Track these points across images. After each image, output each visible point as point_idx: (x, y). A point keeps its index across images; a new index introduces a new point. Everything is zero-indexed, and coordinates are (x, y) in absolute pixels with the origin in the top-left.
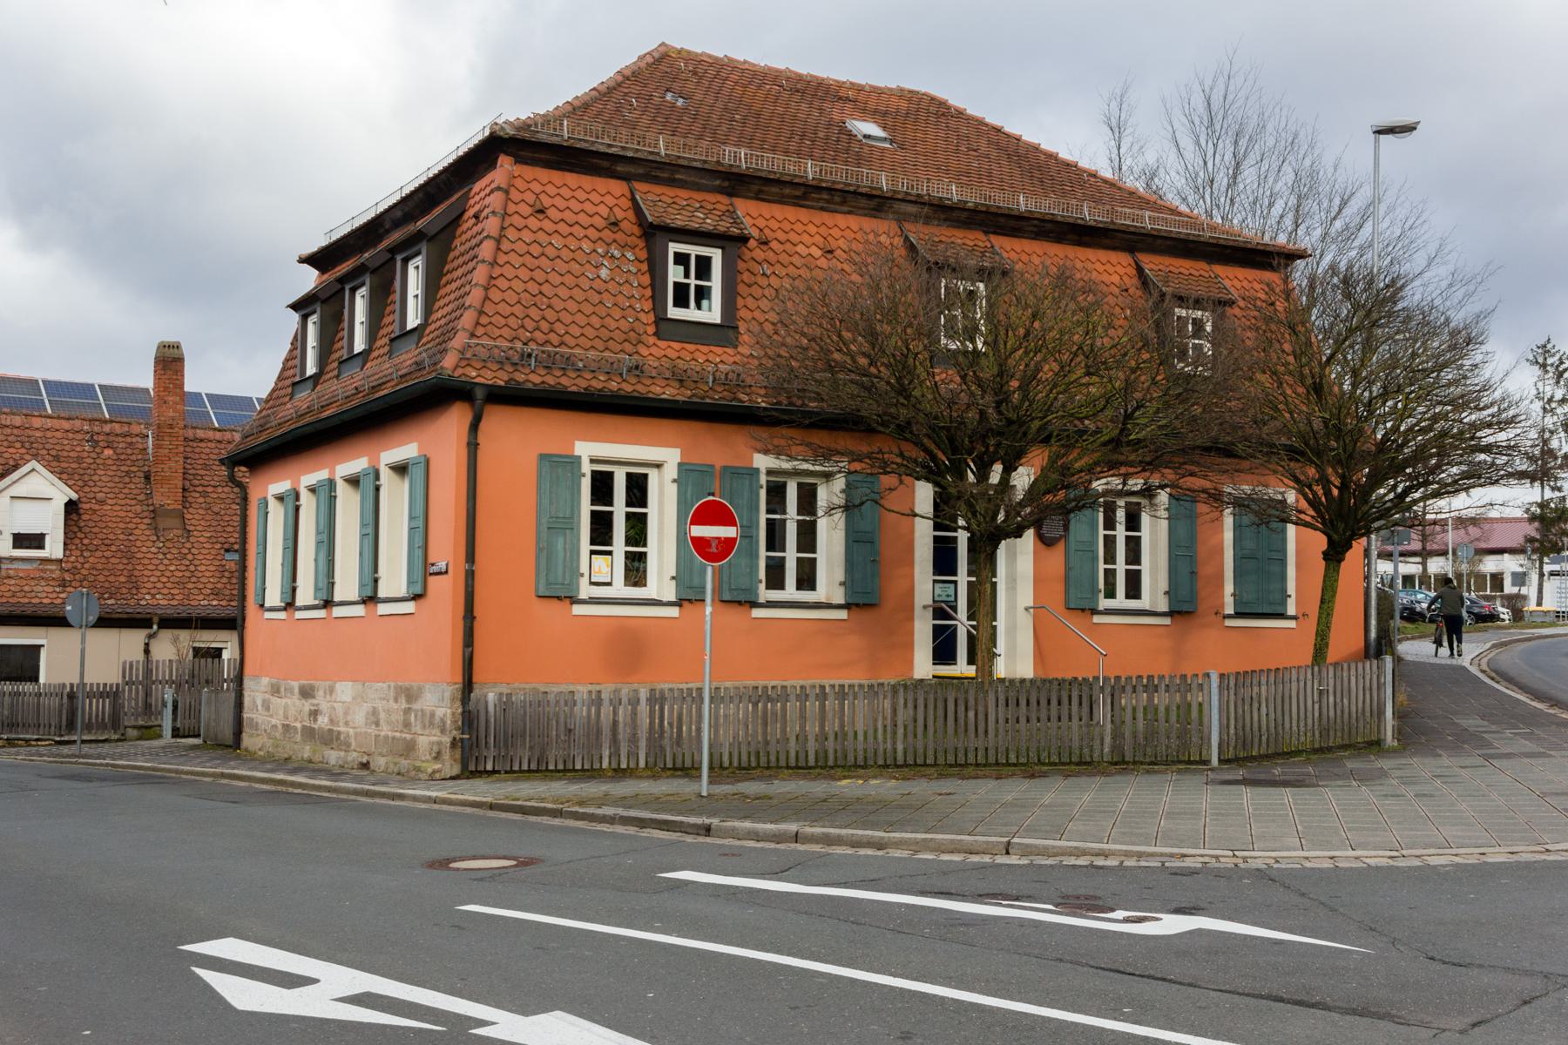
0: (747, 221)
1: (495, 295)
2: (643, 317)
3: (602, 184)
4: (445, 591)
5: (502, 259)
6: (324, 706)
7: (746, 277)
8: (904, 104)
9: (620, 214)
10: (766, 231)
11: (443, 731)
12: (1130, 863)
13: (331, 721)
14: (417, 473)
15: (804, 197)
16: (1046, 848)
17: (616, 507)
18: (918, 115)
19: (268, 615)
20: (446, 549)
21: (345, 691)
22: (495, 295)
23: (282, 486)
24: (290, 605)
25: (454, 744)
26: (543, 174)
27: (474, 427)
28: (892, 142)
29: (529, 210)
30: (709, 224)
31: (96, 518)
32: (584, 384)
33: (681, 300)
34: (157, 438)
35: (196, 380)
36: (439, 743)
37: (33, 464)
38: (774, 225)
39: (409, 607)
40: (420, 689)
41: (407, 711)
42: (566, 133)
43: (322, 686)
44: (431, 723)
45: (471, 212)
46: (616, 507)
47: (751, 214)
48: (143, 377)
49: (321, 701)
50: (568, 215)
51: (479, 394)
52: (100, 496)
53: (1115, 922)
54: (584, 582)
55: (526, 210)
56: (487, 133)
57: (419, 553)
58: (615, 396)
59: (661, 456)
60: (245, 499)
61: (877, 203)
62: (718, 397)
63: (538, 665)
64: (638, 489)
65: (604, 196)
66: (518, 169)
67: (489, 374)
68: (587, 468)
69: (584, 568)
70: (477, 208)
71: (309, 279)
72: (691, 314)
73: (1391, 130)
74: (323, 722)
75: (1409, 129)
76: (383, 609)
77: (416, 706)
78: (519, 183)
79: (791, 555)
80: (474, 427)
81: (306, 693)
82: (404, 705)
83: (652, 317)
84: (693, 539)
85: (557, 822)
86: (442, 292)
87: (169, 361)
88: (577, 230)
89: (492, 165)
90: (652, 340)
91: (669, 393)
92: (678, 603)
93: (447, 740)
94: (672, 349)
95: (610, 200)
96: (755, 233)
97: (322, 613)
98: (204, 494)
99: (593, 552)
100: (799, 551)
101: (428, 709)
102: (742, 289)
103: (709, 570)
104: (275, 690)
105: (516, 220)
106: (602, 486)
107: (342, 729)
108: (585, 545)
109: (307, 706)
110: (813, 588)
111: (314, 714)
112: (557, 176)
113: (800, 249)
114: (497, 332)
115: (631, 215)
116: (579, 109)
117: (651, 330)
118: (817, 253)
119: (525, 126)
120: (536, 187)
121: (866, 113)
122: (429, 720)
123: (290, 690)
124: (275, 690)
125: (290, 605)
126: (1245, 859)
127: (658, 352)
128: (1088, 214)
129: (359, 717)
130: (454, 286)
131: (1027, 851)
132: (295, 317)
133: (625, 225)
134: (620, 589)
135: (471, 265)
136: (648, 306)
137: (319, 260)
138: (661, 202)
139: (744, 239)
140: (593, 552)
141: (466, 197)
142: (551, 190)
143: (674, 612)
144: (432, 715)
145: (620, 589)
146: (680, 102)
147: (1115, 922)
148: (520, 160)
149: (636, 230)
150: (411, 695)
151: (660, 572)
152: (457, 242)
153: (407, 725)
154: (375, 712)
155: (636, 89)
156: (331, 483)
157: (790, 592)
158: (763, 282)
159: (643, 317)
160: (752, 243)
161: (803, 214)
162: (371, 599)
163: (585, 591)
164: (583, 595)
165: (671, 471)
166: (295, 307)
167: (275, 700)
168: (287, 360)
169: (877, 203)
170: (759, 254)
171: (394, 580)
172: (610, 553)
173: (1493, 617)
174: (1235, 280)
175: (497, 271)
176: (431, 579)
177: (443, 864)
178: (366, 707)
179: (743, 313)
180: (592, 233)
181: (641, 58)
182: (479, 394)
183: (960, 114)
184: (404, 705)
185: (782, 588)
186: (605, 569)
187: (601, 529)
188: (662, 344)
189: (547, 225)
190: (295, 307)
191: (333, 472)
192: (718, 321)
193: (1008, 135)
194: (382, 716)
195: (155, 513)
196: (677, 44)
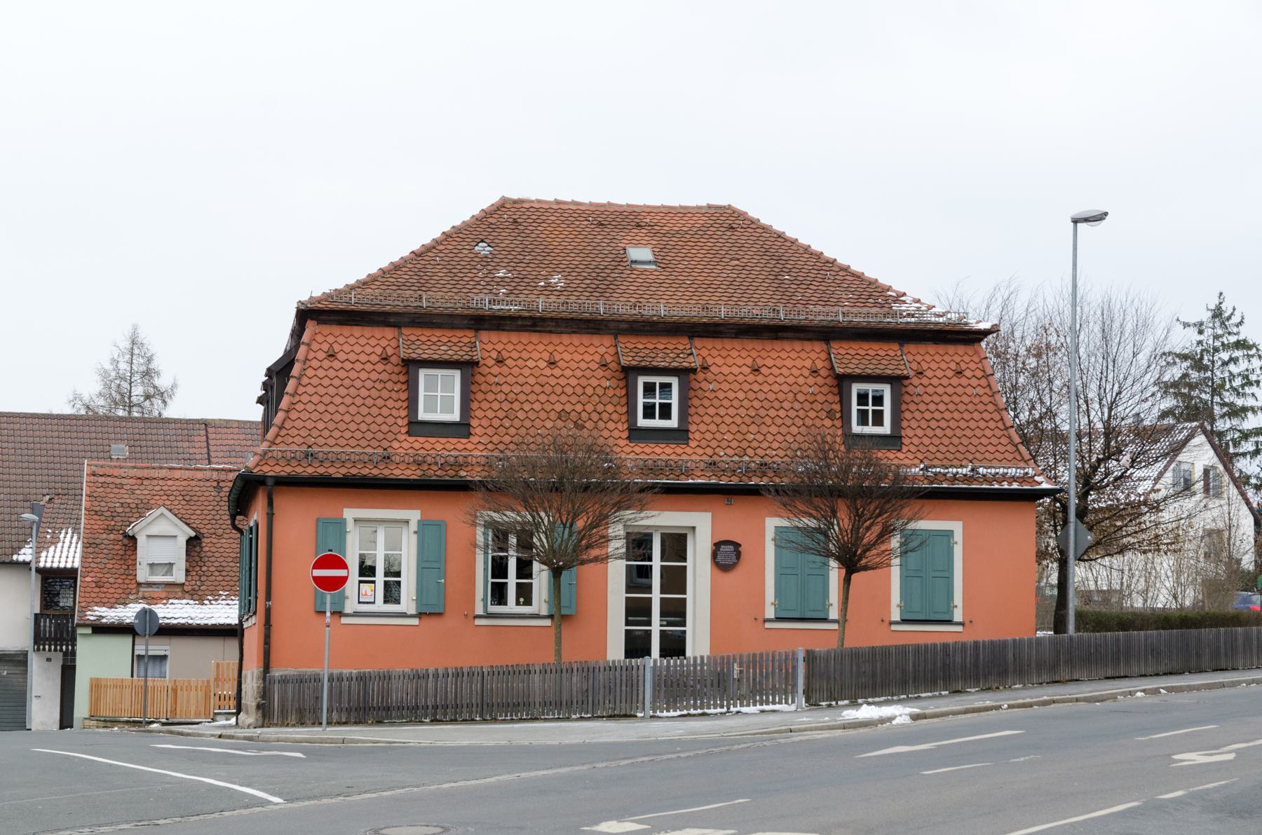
5: (301, 390)
10: (504, 353)
15: (534, 325)
22: (294, 415)
26: (336, 330)
29: (324, 355)
31: (214, 549)
37: (162, 510)
47: (487, 345)
51: (270, 482)
58: (364, 477)
62: (435, 473)
66: (319, 328)
73: (1086, 220)
75: (1102, 217)
76: (344, 620)
79: (512, 580)
91: (412, 474)
92: (420, 615)
99: (360, 582)
100: (518, 578)
103: (328, 598)
105: (315, 364)
110: (398, 601)
119: (327, 297)
127: (405, 446)
132: (261, 408)
134: (380, 606)
143: (415, 621)
145: (380, 606)
148: (320, 322)
157: (512, 606)
159: (400, 422)
161: (535, 338)
172: (374, 582)
175: (297, 398)
182: (270, 482)
185: (506, 604)
188: (411, 439)
192: (458, 419)
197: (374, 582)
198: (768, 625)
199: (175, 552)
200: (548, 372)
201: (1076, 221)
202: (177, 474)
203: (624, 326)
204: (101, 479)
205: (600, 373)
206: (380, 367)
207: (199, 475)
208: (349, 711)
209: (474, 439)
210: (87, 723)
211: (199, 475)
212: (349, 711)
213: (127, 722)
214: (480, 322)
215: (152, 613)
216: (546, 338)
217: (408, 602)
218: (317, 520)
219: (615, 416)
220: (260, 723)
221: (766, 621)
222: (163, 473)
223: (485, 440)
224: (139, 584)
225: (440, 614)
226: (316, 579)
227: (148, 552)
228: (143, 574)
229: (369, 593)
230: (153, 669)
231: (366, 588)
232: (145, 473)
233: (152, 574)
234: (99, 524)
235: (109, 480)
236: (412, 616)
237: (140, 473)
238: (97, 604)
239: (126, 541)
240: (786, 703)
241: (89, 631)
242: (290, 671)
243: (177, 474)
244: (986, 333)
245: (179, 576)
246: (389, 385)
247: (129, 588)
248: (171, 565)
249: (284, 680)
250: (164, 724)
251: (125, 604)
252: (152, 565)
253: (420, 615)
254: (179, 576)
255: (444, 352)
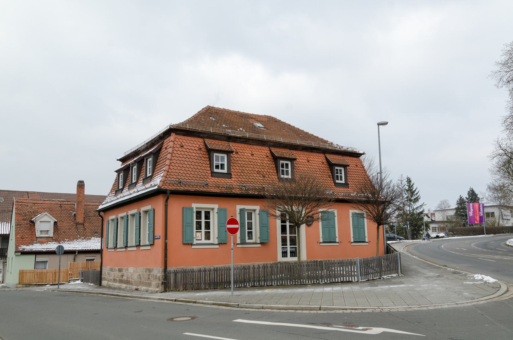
0: (233, 148)
1: (171, 167)
2: (208, 172)
3: (197, 139)
4: (160, 243)
6: (125, 274)
7: (233, 161)
8: (266, 119)
9: (201, 147)
11: (159, 280)
12: (353, 311)
13: (127, 278)
14: (152, 213)
15: (246, 141)
16: (330, 308)
17: (203, 220)
18: (270, 122)
19: (109, 250)
20: (159, 232)
21: (131, 270)
23: (113, 217)
24: (116, 248)
25: (162, 283)
27: (167, 201)
28: (265, 128)
30: (224, 149)
32: (194, 189)
33: (217, 167)
34: (78, 205)
35: (88, 191)
36: (158, 283)
37: (46, 213)
38: (239, 148)
39: (149, 248)
40: (153, 269)
41: (149, 275)
42: (183, 127)
43: (124, 268)
44: (156, 278)
45: (164, 147)
46: (203, 220)
47: (233, 146)
48: (74, 191)
49: (124, 272)
50: (189, 147)
51: (168, 192)
52: (63, 220)
53: (359, 330)
54: (195, 239)
55: (178, 146)
56: (168, 128)
57: (152, 234)
58: (202, 192)
59: (214, 206)
60: (103, 220)
61: (262, 143)
62: (224, 191)
63: (183, 261)
64: (207, 217)
65: (197, 143)
67: (171, 187)
68: (195, 210)
69: (195, 236)
70: (166, 146)
71: (119, 165)
72: (220, 171)
73: (382, 124)
74: (125, 278)
75: (386, 123)
76: (142, 248)
77: (152, 273)
78: (177, 140)
80: (167, 201)
81: (120, 270)
82: (148, 273)
83: (210, 172)
84: (228, 228)
85: (195, 305)
86: (157, 167)
87: (81, 185)
88: (191, 151)
89: (170, 135)
90: (210, 177)
92: (219, 244)
93: (160, 282)
94: (216, 179)
95: (199, 143)
96: (235, 150)
97: (124, 250)
98: (89, 219)
99: (197, 232)
101: (155, 274)
102: (232, 164)
103: (232, 237)
104: (111, 270)
105: (176, 149)
106: (199, 213)
107: (130, 280)
108: (195, 230)
109: (120, 274)
111: (122, 276)
112: (186, 138)
113: (246, 154)
114: (172, 177)
115: (204, 147)
116: (190, 121)
117: (210, 175)
118: (250, 155)
120: (181, 140)
121: (260, 122)
122: (156, 277)
123: (115, 270)
124: (111, 270)
125: (116, 248)
126: (382, 309)
127: (212, 181)
128: (313, 144)
129: (135, 277)
130: (160, 165)
131: (325, 309)
132: (116, 174)
133: (202, 149)
134: (204, 241)
135: (165, 160)
136: (209, 169)
137: (123, 160)
138: (212, 144)
139: (232, 152)
140: (197, 232)
141: (163, 143)
142: (185, 141)
143: (217, 247)
144: (156, 276)
145: (204, 241)
146: (214, 119)
147: (359, 330)
149: (206, 150)
150: (150, 271)
151: (214, 236)
152: (161, 154)
153: (149, 278)
154: (140, 275)
155: (203, 116)
156: (128, 216)
158: (237, 162)
159: (208, 172)
160: (234, 153)
161: (246, 146)
162: (139, 246)
163: (195, 242)
164: (195, 243)
165: (216, 211)
166: (116, 171)
167: (111, 272)
168: (114, 185)
169: (262, 143)
170: (236, 156)
171: (145, 240)
172: (201, 232)
173: (75, 215)
174: (347, 160)
175: (172, 161)
176: (156, 240)
177: (172, 319)
178: (137, 274)
179: (232, 170)
180: (195, 151)
181: (203, 109)
182: (168, 192)
183: (280, 121)
184: (148, 273)
186: (199, 236)
187: (199, 226)
189: (184, 150)
190: (116, 171)
191: (127, 213)
193: (292, 126)
194: (142, 276)
195: (77, 224)
196: (212, 106)
197: (201, 232)
198: (321, 244)
199: (50, 227)
200: (251, 157)
201: (379, 124)
202: (47, 202)
203: (272, 144)
204: (20, 203)
205: (266, 159)
206: (199, 152)
207: (54, 202)
208: (210, 284)
209: (233, 179)
210: (18, 286)
211: (54, 202)
212: (210, 284)
213: (36, 285)
214: (230, 139)
215: (62, 247)
216: (250, 146)
217: (214, 238)
218: (183, 208)
219: (273, 174)
220: (163, 290)
221: (320, 243)
222: (42, 202)
223: (236, 179)
224: (37, 238)
225: (225, 244)
226: (229, 229)
227: (39, 227)
228: (38, 234)
229: (200, 236)
230: (41, 266)
231: (198, 234)
232: (35, 202)
233: (41, 234)
234: (20, 218)
235: (23, 204)
236: (134, 247)
237: (34, 202)
238: (22, 244)
239: (31, 223)
240: (254, 268)
241: (20, 254)
242: (180, 268)
243: (47, 202)
244: (361, 154)
245: (52, 235)
246: (203, 158)
247: (34, 239)
248: (48, 231)
249: (176, 273)
250: (51, 285)
251: (32, 244)
252: (41, 231)
253: (219, 244)
254: (51, 234)
255: (221, 148)
